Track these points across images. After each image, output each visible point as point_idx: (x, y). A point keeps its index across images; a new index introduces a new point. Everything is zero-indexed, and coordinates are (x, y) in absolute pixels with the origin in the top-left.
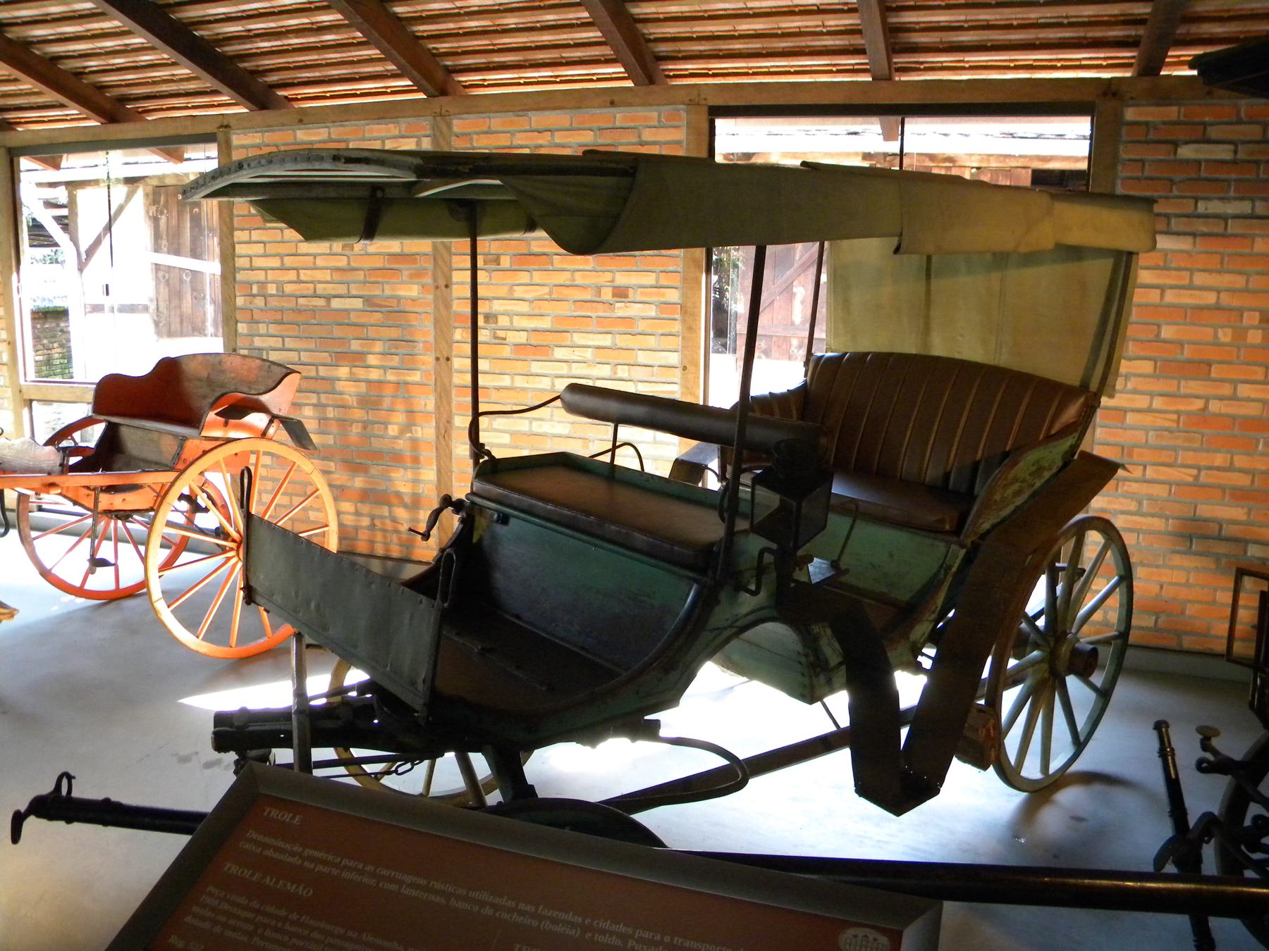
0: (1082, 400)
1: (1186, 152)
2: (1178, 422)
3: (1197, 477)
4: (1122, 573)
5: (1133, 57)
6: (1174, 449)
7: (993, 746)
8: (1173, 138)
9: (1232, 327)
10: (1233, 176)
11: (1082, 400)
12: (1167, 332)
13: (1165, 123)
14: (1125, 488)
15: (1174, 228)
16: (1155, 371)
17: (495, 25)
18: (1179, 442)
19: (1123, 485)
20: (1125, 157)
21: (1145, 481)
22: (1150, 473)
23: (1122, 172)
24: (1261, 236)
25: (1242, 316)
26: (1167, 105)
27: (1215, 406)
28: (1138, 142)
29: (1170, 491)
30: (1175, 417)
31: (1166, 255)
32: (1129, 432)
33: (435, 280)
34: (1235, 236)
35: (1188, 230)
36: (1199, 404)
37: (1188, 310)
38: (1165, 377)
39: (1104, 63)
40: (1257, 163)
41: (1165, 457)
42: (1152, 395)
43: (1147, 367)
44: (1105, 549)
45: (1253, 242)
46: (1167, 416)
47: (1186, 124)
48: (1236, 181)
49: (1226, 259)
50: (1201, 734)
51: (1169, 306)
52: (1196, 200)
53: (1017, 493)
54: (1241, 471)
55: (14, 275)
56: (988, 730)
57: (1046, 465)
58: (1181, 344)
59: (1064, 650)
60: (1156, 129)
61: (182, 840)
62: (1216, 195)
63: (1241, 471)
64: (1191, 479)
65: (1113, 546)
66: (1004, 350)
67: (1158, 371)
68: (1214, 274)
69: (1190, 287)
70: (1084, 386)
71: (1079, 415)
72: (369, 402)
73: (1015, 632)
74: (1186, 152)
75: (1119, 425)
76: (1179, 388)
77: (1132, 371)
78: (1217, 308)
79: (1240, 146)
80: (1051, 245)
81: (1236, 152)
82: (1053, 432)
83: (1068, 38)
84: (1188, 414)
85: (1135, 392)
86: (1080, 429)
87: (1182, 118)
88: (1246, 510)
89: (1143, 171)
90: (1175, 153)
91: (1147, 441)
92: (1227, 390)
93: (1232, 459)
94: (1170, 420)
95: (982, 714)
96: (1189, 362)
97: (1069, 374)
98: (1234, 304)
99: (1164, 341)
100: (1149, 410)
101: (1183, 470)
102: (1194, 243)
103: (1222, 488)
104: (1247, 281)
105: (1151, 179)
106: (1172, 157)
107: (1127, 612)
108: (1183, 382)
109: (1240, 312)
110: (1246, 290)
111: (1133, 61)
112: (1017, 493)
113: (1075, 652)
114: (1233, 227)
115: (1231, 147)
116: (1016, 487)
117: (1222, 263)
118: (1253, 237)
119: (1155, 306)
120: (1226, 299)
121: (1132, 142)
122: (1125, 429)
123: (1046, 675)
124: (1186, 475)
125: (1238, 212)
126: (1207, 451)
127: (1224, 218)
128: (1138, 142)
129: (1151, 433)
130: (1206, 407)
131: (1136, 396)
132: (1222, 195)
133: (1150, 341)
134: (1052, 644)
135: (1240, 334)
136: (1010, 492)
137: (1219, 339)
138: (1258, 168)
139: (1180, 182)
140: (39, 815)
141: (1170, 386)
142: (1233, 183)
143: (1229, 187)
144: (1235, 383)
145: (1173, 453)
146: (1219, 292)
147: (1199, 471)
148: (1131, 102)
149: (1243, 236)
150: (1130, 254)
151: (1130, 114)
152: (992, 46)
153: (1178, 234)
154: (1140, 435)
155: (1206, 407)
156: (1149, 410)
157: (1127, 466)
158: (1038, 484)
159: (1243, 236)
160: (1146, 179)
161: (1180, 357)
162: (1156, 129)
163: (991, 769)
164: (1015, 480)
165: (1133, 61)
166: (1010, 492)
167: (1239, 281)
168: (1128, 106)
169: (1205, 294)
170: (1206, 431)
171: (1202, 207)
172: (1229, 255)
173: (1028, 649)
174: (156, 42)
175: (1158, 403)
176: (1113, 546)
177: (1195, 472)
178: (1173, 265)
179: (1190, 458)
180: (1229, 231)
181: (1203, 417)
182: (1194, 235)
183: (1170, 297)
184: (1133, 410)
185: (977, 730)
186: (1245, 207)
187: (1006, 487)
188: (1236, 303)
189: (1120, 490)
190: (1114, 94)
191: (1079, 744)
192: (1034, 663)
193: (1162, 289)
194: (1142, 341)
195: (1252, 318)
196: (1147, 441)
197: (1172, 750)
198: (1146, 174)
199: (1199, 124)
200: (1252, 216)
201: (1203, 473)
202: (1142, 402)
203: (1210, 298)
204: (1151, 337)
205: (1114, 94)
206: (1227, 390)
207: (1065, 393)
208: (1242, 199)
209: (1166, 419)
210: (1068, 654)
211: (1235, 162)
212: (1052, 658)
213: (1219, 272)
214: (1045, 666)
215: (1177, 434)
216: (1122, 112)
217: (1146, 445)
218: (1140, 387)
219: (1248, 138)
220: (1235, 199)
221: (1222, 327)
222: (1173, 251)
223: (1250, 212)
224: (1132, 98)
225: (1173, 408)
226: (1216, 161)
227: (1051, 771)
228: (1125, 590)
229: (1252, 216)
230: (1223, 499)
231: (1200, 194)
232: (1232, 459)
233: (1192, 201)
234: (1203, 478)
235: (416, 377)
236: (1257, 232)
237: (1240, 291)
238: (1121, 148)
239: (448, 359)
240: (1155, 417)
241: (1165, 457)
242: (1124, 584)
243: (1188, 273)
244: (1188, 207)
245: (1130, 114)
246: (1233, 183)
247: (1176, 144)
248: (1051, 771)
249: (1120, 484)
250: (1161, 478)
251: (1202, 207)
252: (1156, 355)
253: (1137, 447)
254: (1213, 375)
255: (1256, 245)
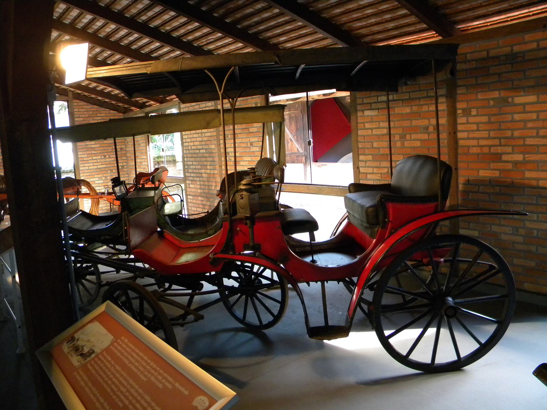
2: (381, 177)
15: (373, 107)
17: (363, 15)
33: (217, 143)
42: (373, 167)
43: (370, 157)
46: (378, 175)
52: (378, 96)
55: (148, 147)
61: (172, 288)
69: (379, 128)
72: (208, 178)
100: (373, 173)
102: (379, 112)
119: (371, 136)
129: (374, 181)
140: (116, 178)
152: (473, 8)
161: (379, 154)
174: (307, 23)
182: (378, 109)
193: (372, 129)
225: (380, 172)
233: (376, 97)
235: (216, 172)
239: (221, 166)
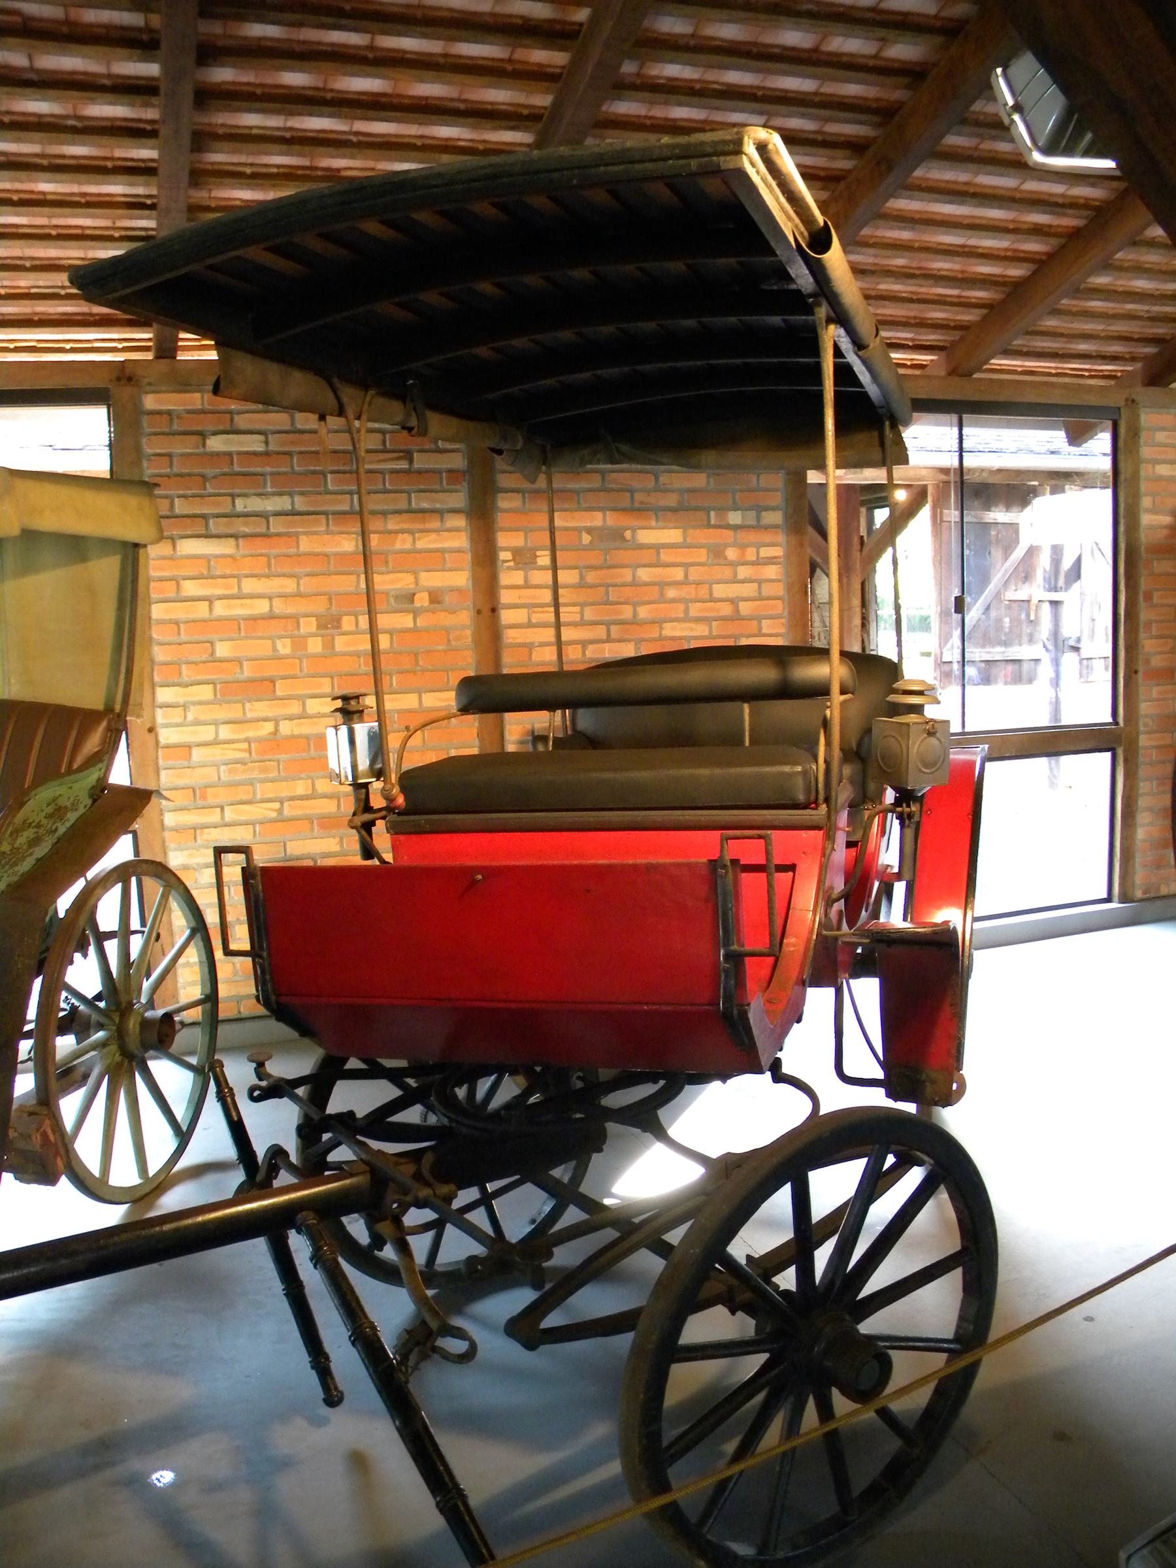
0: (104, 724)
1: (216, 444)
3: (280, 811)
4: (193, 924)
5: (149, 340)
6: (251, 783)
7: (57, 1153)
8: (199, 428)
9: (291, 637)
10: (268, 469)
11: (104, 724)
12: (223, 650)
13: (189, 412)
14: (205, 837)
16: (215, 695)
18: (255, 774)
19: (202, 833)
20: (150, 451)
21: (226, 825)
22: (229, 815)
23: (148, 468)
24: (305, 533)
25: (298, 623)
26: (188, 392)
27: (286, 728)
28: (164, 434)
29: (255, 832)
30: (245, 745)
31: (209, 561)
32: (198, 771)
34: (278, 535)
35: (231, 531)
36: (269, 727)
37: (242, 622)
38: (229, 702)
39: (120, 346)
40: (289, 454)
41: (243, 793)
42: (216, 723)
44: (165, 897)
45: (298, 543)
47: (212, 412)
48: (272, 474)
49: (273, 562)
50: (253, 1061)
51: (219, 619)
52: (233, 496)
53: (35, 842)
54: (325, 796)
56: (45, 1135)
57: (68, 804)
58: (239, 661)
59: (132, 1024)
60: (179, 417)
62: (253, 491)
63: (325, 796)
64: (274, 815)
65: (173, 892)
66: (13, 681)
67: (219, 696)
68: (263, 579)
69: (239, 597)
70: (109, 709)
71: (104, 742)
73: (758, 1337)
74: (216, 444)
75: (186, 763)
76: (244, 713)
77: (190, 699)
78: (271, 616)
79: (270, 436)
80: (16, 532)
81: (267, 443)
82: (75, 766)
83: (71, 314)
84: (259, 740)
85: (197, 723)
86: (106, 758)
87: (207, 407)
88: (337, 839)
89: (171, 466)
90: (204, 445)
91: (219, 778)
92: (294, 708)
93: (313, 785)
94: (240, 750)
95: (34, 1117)
96: (252, 681)
97: (93, 700)
98: (289, 611)
99: (221, 661)
100: (216, 742)
101: (264, 805)
102: (237, 546)
103: (310, 819)
104: (298, 584)
105: (181, 475)
106: (201, 450)
107: (210, 967)
108: (248, 705)
109: (295, 618)
110: (299, 595)
111: (150, 344)
112: (35, 842)
113: (146, 1024)
114: (276, 525)
115: (261, 438)
116: (29, 834)
117: (269, 566)
118: (297, 535)
120: (279, 607)
121: (155, 434)
122: (194, 768)
123: (118, 1058)
124: (267, 811)
125: (278, 508)
126: (286, 780)
127: (264, 516)
128: (164, 434)
129: (223, 768)
130: (276, 731)
131: (200, 728)
132: (260, 491)
133: (204, 662)
134: (117, 1020)
135: (299, 642)
136: (22, 840)
137: (278, 651)
138: (292, 461)
139: (213, 478)
141: (235, 712)
142: (268, 477)
143: (265, 480)
144: (302, 699)
145: (250, 787)
146: (271, 598)
147: (282, 803)
148: (148, 388)
149: (288, 535)
150: (136, 546)
151: (150, 402)
153: (218, 536)
154: (210, 774)
155: (276, 731)
156: (216, 742)
157: (164, 793)
158: (62, 830)
159: (288, 535)
160: (176, 475)
162: (179, 417)
163: (64, 1181)
164: (26, 825)
165: (150, 344)
166: (22, 840)
167: (290, 585)
168: (147, 393)
169: (256, 601)
170: (283, 757)
171: (240, 505)
172: (277, 556)
173: (92, 1032)
175: (225, 732)
176: (173, 892)
177: (277, 805)
178: (218, 573)
179: (269, 790)
180: (272, 530)
181: (275, 742)
182: (235, 536)
183: (220, 609)
184: (199, 745)
185: (30, 1136)
186: (283, 503)
187: (16, 833)
188: (290, 610)
189: (199, 841)
190: (130, 379)
191: (184, 1136)
192: (102, 1045)
193: (210, 600)
194: (196, 663)
195: (309, 626)
196: (219, 778)
197: (231, 1089)
198: (175, 470)
199: (225, 412)
200: (293, 513)
201: (286, 804)
202: (207, 733)
203: (262, 607)
204: (205, 657)
205: (130, 379)
206: (294, 708)
207: (85, 719)
208: (280, 494)
209: (235, 749)
210: (138, 1027)
211: (267, 454)
212: (120, 1035)
213: (268, 577)
214: (113, 1048)
215: (250, 765)
216: (141, 402)
217: (219, 784)
218: (202, 717)
219: (278, 428)
220: (274, 494)
221: (280, 637)
222: (217, 556)
223: (290, 508)
224: (150, 384)
225: (242, 736)
226: (247, 453)
227: (151, 1173)
228: (201, 944)
229: (293, 513)
230: (312, 829)
231: (238, 491)
232: (313, 785)
234: (287, 812)
236: (301, 530)
237: (293, 596)
238: (144, 440)
240: (223, 749)
241: (243, 793)
242: (198, 936)
243: (236, 580)
244: (225, 506)
245: (150, 402)
246: (268, 477)
247: (203, 435)
248: (151, 1173)
249: (198, 832)
250: (243, 818)
251: (240, 505)
252: (215, 677)
253: (210, 786)
254: (279, 693)
255: (301, 543)
